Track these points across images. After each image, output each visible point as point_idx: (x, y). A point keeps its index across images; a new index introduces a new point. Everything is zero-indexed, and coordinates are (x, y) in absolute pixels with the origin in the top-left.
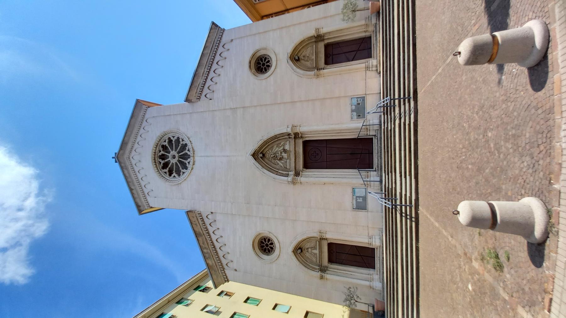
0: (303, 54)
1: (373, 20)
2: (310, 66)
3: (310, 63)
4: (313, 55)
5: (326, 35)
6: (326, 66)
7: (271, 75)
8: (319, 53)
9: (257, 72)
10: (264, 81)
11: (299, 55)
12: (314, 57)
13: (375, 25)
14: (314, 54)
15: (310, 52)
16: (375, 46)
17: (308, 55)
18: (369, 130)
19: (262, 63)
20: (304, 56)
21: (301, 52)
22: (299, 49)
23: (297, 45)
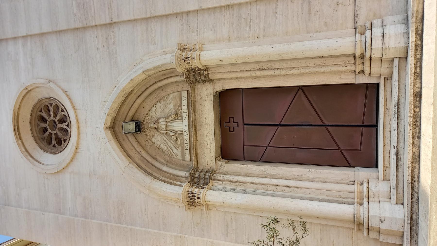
19: (49, 120)
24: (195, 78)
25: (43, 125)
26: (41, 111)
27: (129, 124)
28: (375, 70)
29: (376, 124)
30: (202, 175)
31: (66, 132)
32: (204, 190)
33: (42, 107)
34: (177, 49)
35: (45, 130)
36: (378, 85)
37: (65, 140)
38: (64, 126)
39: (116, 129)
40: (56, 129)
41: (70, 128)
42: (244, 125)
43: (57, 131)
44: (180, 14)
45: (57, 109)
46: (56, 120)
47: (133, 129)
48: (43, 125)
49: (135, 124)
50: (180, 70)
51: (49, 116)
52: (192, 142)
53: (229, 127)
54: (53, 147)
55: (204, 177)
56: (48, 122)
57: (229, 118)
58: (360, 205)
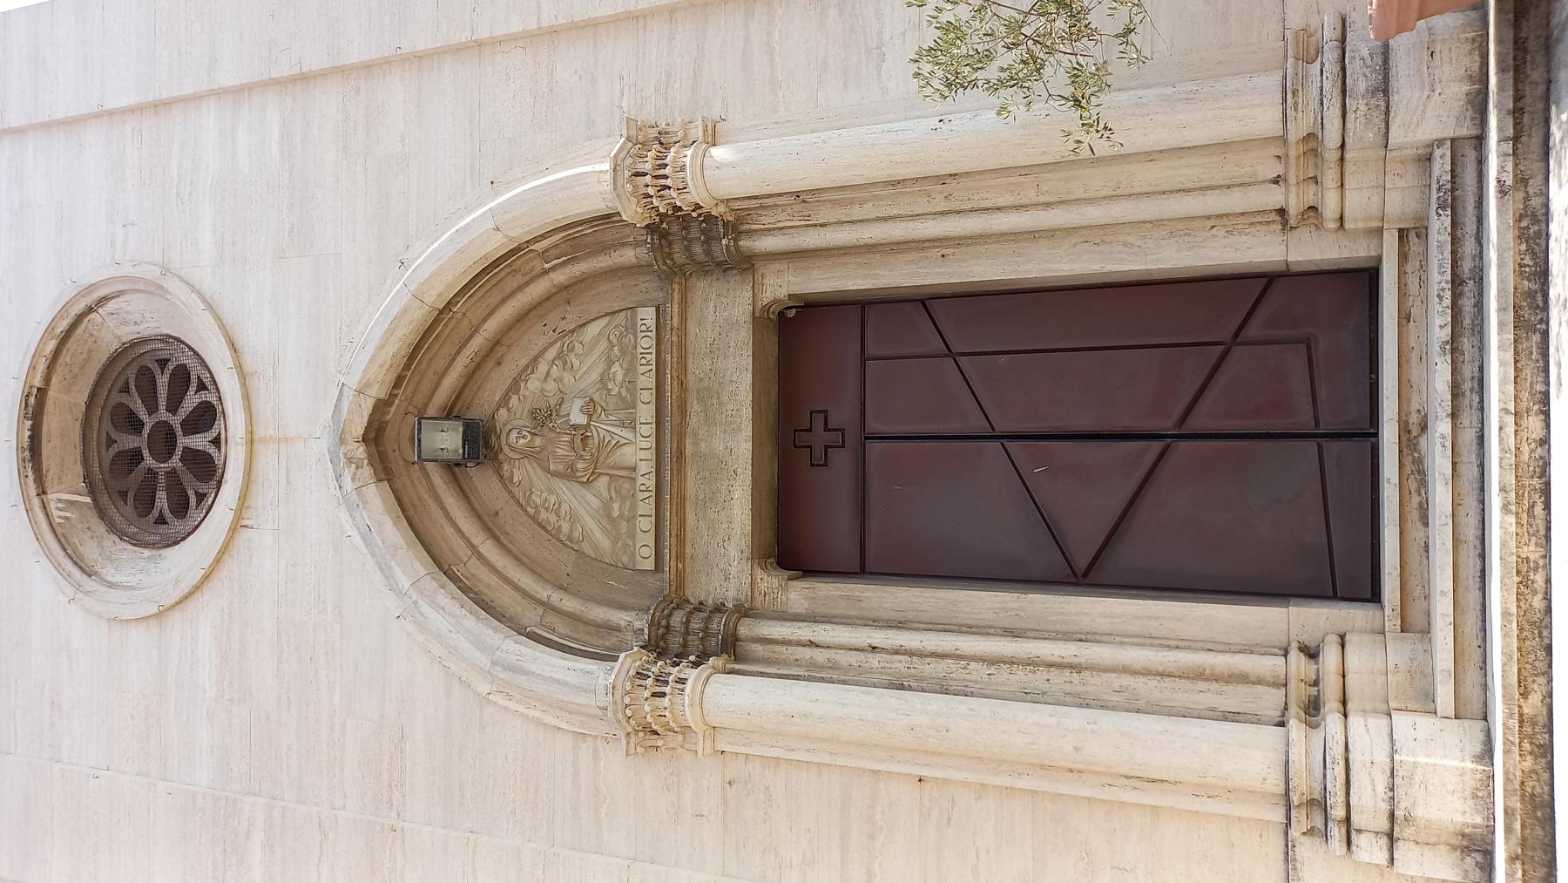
0: (534, 384)
1: (1405, 93)
2: (605, 543)
3: (607, 509)
4: (631, 425)
5: (768, 220)
6: (770, 581)
7: (217, 561)
8: (694, 407)
9: (102, 514)
10: (137, 634)
11: (484, 402)
12: (638, 450)
13: (1441, 166)
14: (646, 413)
15: (603, 381)
16: (1439, 463)
17: (578, 418)
18: (1332, 156)
19: (149, 422)
20: (543, 418)
21: (515, 361)
22: (477, 343)
23: (437, 295)
24: (688, 249)
25: (128, 442)
26: (126, 390)
27: (442, 431)
28: (1360, 201)
29: (1368, 426)
30: (696, 624)
31: (206, 469)
32: (699, 674)
33: (131, 376)
34: (623, 139)
35: (135, 457)
36: (1368, 276)
37: (201, 497)
38: (199, 442)
39: (389, 447)
40: (173, 454)
41: (223, 450)
42: (866, 438)
43: (176, 461)
44: (642, 21)
45: (182, 378)
46: (176, 421)
47: (456, 451)
48: (128, 442)
49: (461, 429)
50: (633, 213)
51: (152, 409)
52: (668, 478)
53: (810, 447)
54: (155, 523)
55: (706, 630)
56: (146, 431)
57: (812, 412)
58: (1310, 727)
